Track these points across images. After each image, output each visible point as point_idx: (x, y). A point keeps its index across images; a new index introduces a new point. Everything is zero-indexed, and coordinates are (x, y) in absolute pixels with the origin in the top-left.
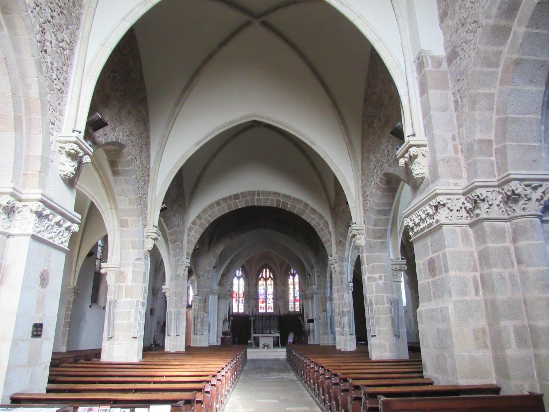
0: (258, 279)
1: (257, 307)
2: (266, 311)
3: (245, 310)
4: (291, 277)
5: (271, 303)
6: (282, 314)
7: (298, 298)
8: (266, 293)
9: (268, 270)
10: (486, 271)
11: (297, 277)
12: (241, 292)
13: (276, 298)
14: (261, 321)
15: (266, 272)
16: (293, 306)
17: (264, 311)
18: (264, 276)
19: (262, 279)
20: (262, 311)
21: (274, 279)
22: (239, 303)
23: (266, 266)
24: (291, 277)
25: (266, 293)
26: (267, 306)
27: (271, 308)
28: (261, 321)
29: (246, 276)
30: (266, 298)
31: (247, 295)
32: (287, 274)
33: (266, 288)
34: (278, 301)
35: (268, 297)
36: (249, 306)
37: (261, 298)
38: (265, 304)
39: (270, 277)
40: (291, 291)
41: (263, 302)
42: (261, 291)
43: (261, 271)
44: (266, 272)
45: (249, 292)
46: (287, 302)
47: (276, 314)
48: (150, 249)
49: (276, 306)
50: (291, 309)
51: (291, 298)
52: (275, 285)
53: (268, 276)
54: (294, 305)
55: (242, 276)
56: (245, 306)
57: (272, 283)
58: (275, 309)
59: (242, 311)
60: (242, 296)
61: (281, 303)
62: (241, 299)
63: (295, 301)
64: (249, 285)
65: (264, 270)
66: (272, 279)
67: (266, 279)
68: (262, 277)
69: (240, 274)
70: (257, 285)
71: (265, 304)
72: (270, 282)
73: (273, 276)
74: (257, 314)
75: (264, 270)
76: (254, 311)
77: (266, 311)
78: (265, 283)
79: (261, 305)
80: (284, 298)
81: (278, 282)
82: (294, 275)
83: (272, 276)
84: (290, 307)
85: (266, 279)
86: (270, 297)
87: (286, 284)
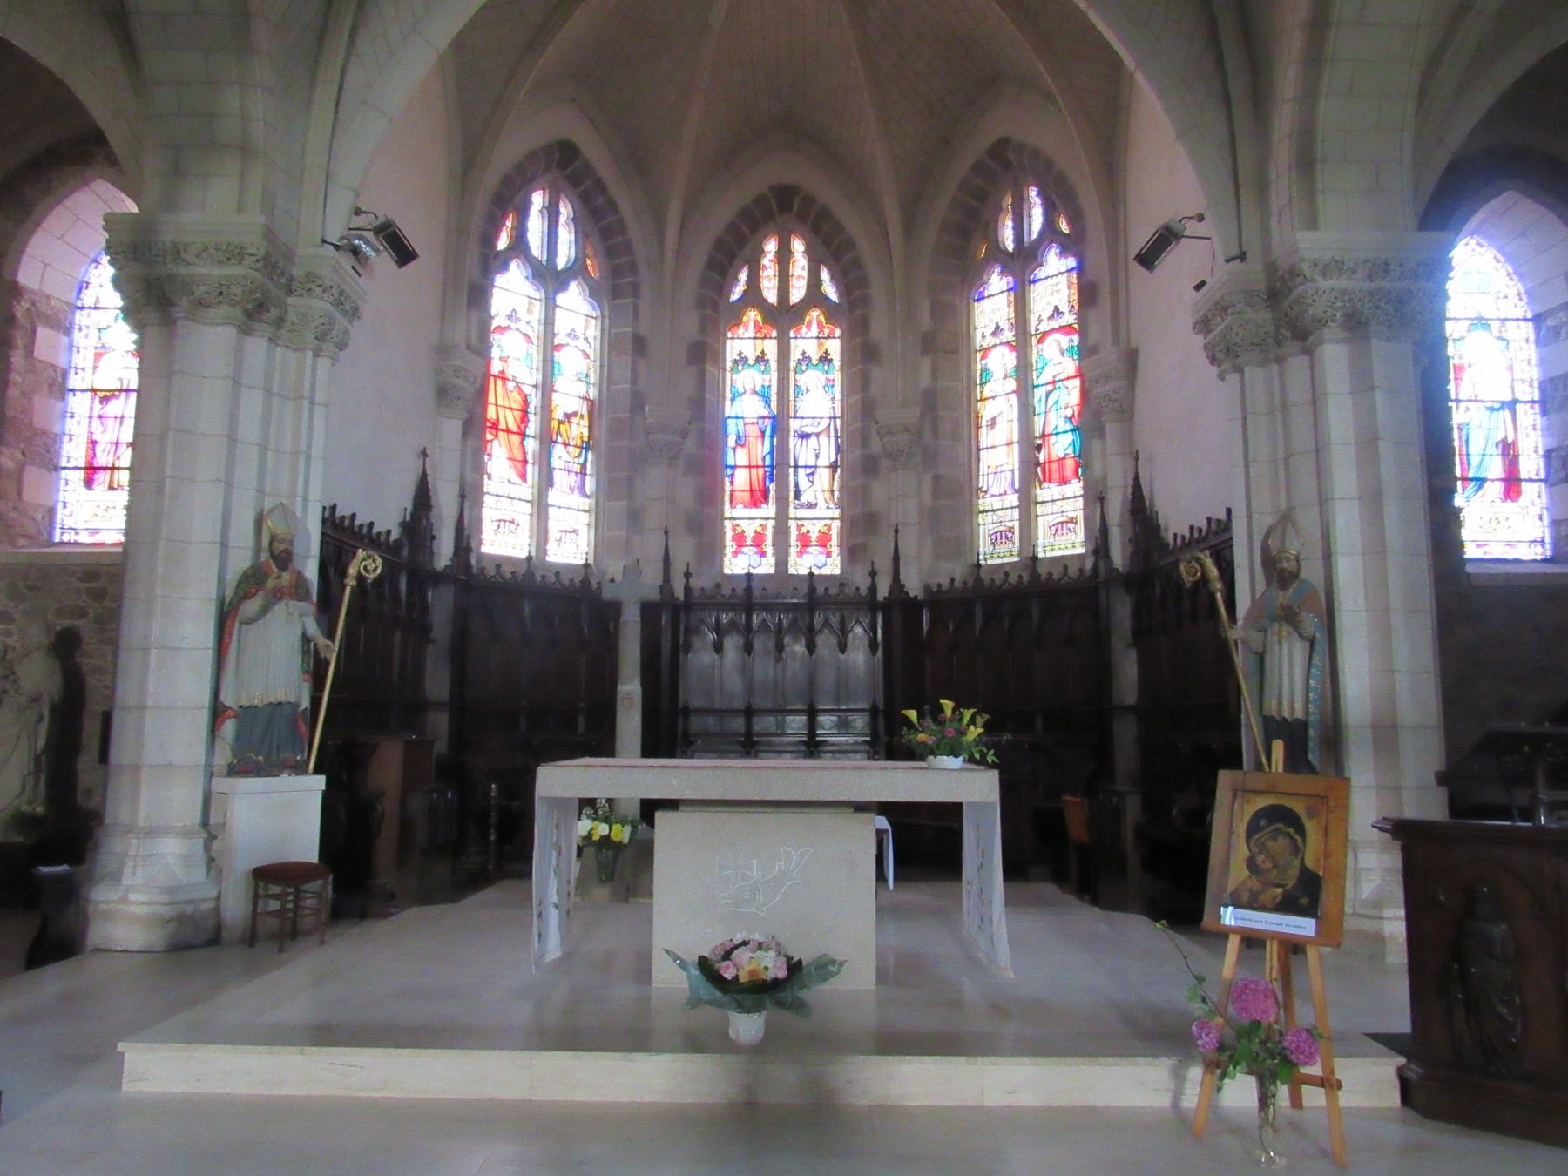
0: (716, 315)
1: (704, 526)
2: (782, 563)
3: (600, 545)
4: (997, 282)
5: (819, 502)
6: (913, 585)
7: (1062, 445)
8: (778, 425)
9: (798, 246)
10: (1234, 942)
11: (1056, 266)
12: (575, 387)
13: (866, 457)
14: (732, 643)
15: (784, 257)
16: (1012, 518)
17: (767, 566)
18: (771, 295)
19: (752, 315)
20: (737, 564)
21: (852, 315)
22: (546, 480)
23: (783, 208)
24: (997, 282)
25: (778, 425)
26: (787, 524)
27: (824, 540)
28: (732, 643)
29: (616, 271)
30: (779, 466)
31: (618, 430)
32: (963, 250)
33: (785, 388)
34: (878, 489)
35: (803, 452)
36: (634, 518)
37: (742, 462)
38: (769, 510)
39: (814, 296)
40: (997, 407)
41: (758, 497)
42: (743, 404)
43: (735, 249)
44: (784, 257)
45: (638, 402)
46: (955, 493)
47: (861, 581)
48: (130, 439)
49: (860, 525)
50: (994, 546)
51: (998, 460)
52: (862, 357)
53: (797, 293)
54: (1027, 505)
55: (576, 270)
56: (600, 518)
57: (834, 347)
58: (852, 553)
59: (571, 544)
60: (579, 429)
61: (905, 497)
62: (561, 457)
63: (1033, 470)
64: (640, 345)
65: (771, 246)
66: (832, 313)
67: (783, 317)
68: (753, 295)
69: (565, 254)
70: (704, 354)
71: (769, 510)
72: (816, 340)
73: (845, 288)
74: (700, 582)
75: (771, 246)
76: (684, 553)
77: (782, 563)
78: (771, 347)
79: (742, 518)
80: (931, 458)
81: (879, 330)
82: (1022, 263)
83: (830, 290)
84: (986, 527)
85: (783, 317)
86: (816, 454)
87: (947, 344)
